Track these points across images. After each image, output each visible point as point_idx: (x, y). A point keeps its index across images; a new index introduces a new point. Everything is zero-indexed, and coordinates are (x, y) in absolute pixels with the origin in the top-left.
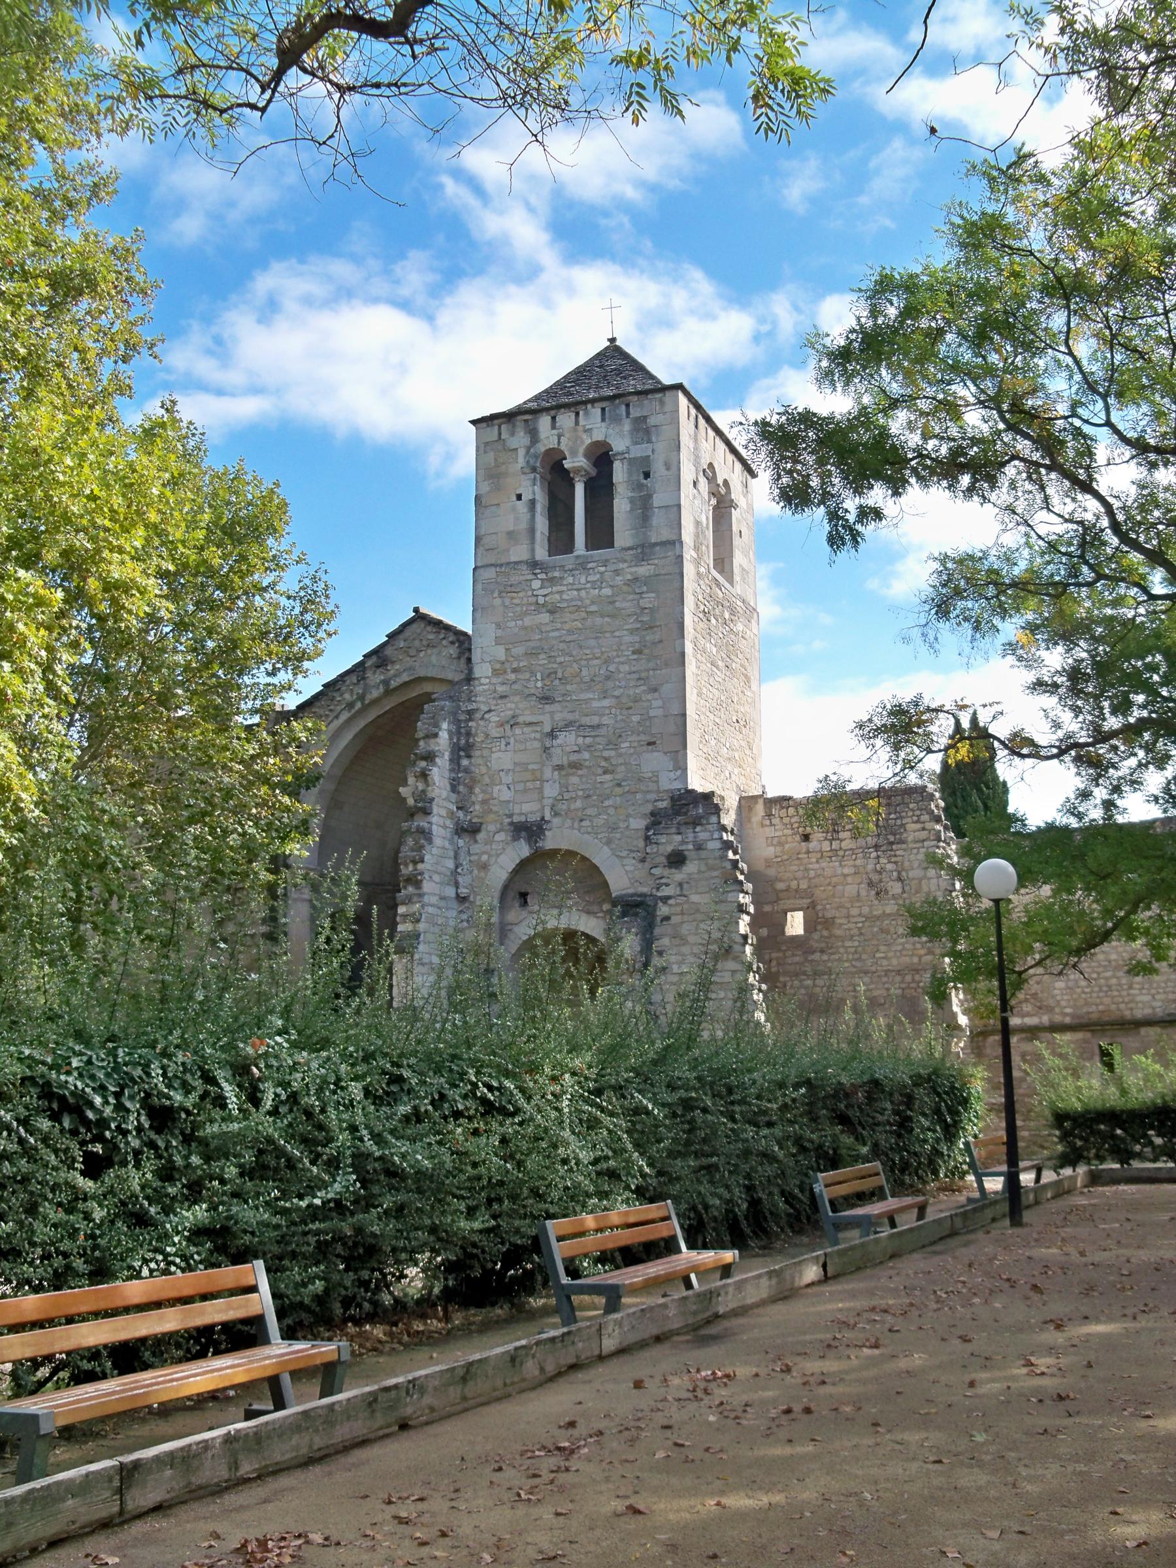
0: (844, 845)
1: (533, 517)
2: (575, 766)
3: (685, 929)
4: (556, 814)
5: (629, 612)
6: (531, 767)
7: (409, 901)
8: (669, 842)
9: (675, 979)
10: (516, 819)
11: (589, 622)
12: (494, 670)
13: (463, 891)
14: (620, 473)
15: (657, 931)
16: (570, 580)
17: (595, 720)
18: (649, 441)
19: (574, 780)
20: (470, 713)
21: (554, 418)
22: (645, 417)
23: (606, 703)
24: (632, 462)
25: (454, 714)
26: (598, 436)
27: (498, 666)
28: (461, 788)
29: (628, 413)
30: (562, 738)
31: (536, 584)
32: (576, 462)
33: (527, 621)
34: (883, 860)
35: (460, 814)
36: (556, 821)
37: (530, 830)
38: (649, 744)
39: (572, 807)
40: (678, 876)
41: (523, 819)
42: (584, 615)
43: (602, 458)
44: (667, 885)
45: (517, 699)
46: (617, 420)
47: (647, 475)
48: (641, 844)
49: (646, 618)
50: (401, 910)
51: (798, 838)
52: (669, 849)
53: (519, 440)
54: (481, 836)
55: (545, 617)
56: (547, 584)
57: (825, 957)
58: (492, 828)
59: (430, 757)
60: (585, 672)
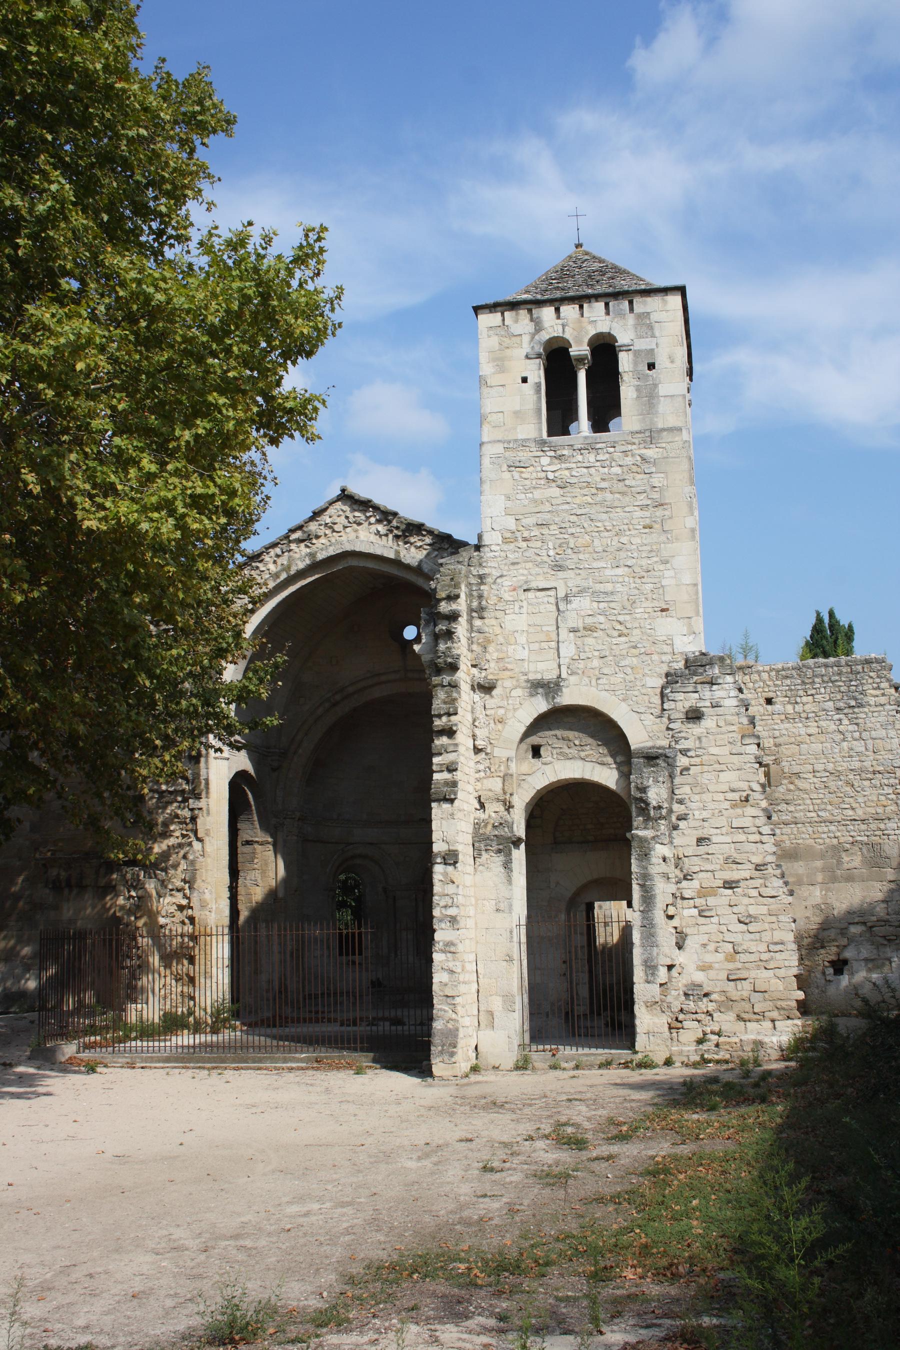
0: (807, 707)
1: (540, 398)
2: (590, 629)
3: (704, 779)
4: (573, 673)
5: (639, 490)
6: (545, 629)
7: (444, 750)
8: (683, 701)
9: (698, 824)
10: (532, 677)
11: (599, 498)
12: (504, 538)
13: (480, 743)
14: (625, 361)
15: (677, 780)
16: (580, 458)
17: (609, 587)
18: (653, 336)
19: (590, 641)
20: (481, 577)
21: (557, 310)
22: (648, 313)
23: (619, 571)
24: (637, 353)
25: (467, 577)
26: (603, 328)
27: (508, 535)
28: (475, 647)
29: (631, 310)
30: (576, 603)
31: (545, 461)
32: (580, 349)
33: (537, 494)
34: (845, 722)
35: (475, 671)
36: (573, 679)
37: (549, 688)
38: (663, 610)
39: (589, 666)
40: (696, 729)
41: (539, 677)
42: (594, 491)
43: (605, 350)
44: (686, 739)
45: (529, 565)
46: (621, 315)
47: (651, 366)
48: (657, 700)
49: (656, 496)
50: (436, 760)
51: (762, 701)
52: (687, 705)
53: (520, 322)
54: (494, 693)
55: (555, 491)
56: (556, 461)
57: (791, 808)
58: (508, 684)
59: (454, 617)
60: (597, 542)
